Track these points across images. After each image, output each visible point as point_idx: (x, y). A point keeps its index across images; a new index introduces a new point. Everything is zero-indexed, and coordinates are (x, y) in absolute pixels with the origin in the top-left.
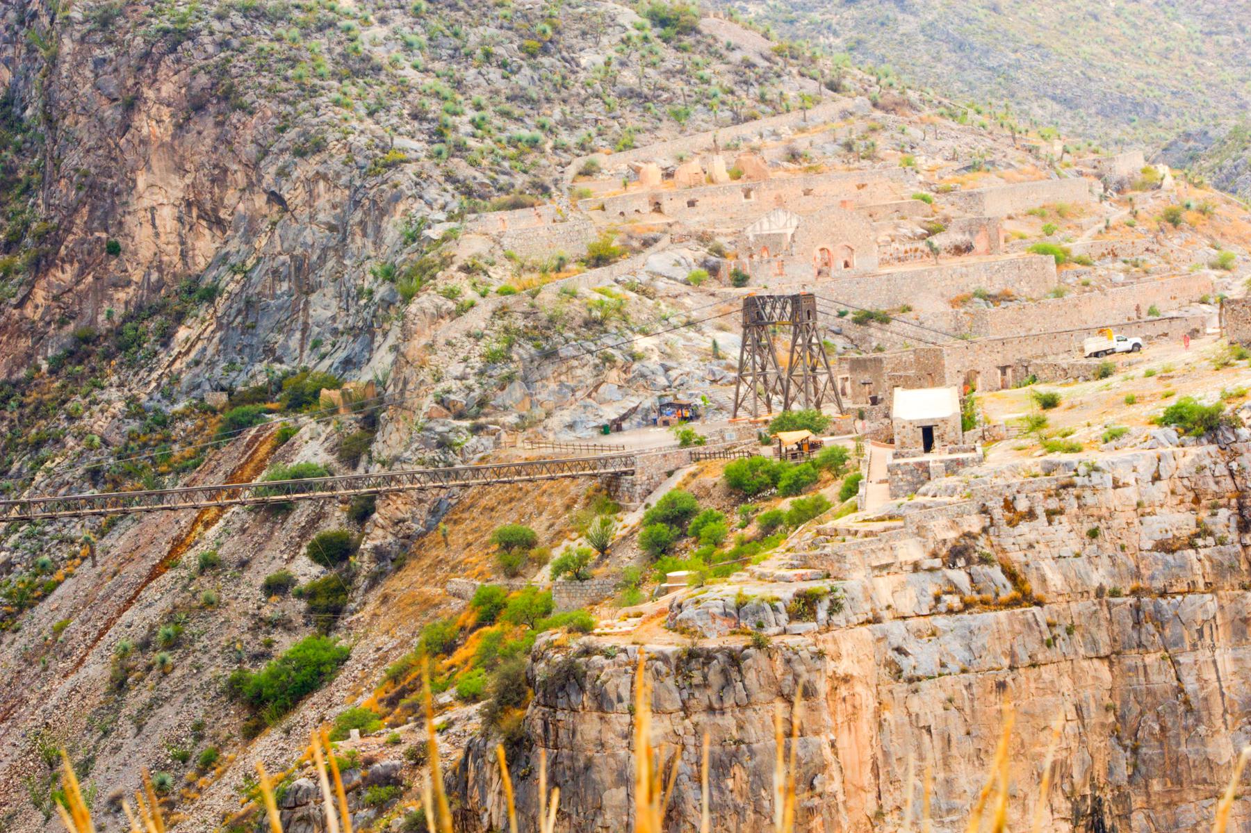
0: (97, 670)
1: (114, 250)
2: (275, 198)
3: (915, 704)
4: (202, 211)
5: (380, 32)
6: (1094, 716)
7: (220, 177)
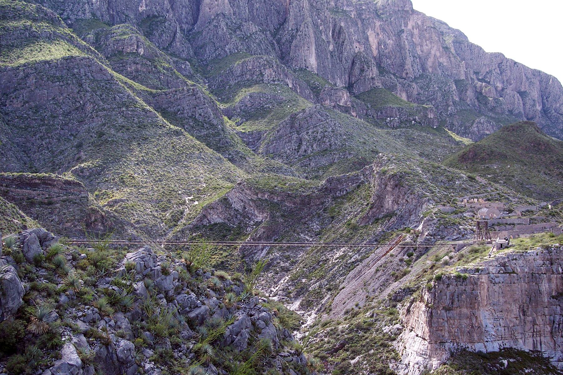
0: (373, 270)
1: (382, 207)
2: (165, 185)
3: (494, 287)
4: (396, 202)
5: (425, 176)
6: (524, 292)
7: (399, 197)
